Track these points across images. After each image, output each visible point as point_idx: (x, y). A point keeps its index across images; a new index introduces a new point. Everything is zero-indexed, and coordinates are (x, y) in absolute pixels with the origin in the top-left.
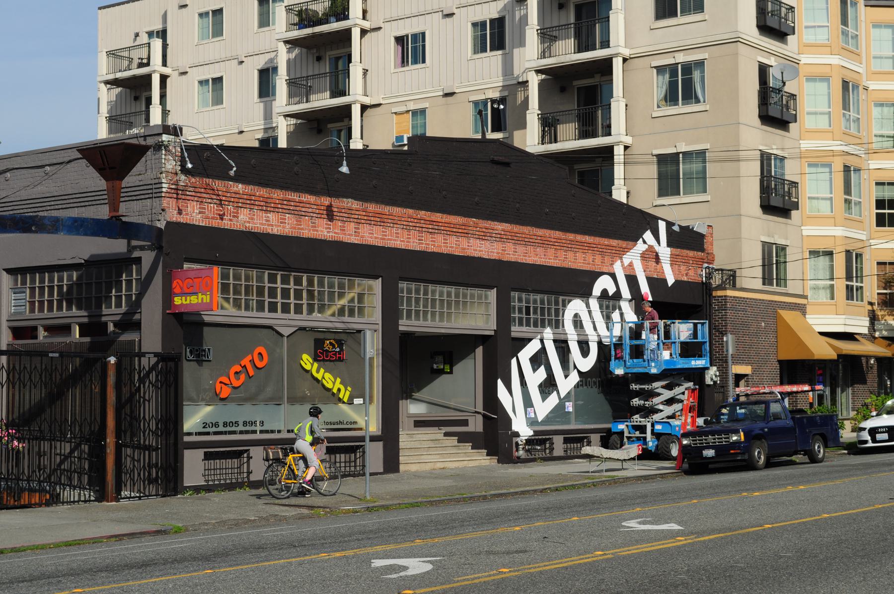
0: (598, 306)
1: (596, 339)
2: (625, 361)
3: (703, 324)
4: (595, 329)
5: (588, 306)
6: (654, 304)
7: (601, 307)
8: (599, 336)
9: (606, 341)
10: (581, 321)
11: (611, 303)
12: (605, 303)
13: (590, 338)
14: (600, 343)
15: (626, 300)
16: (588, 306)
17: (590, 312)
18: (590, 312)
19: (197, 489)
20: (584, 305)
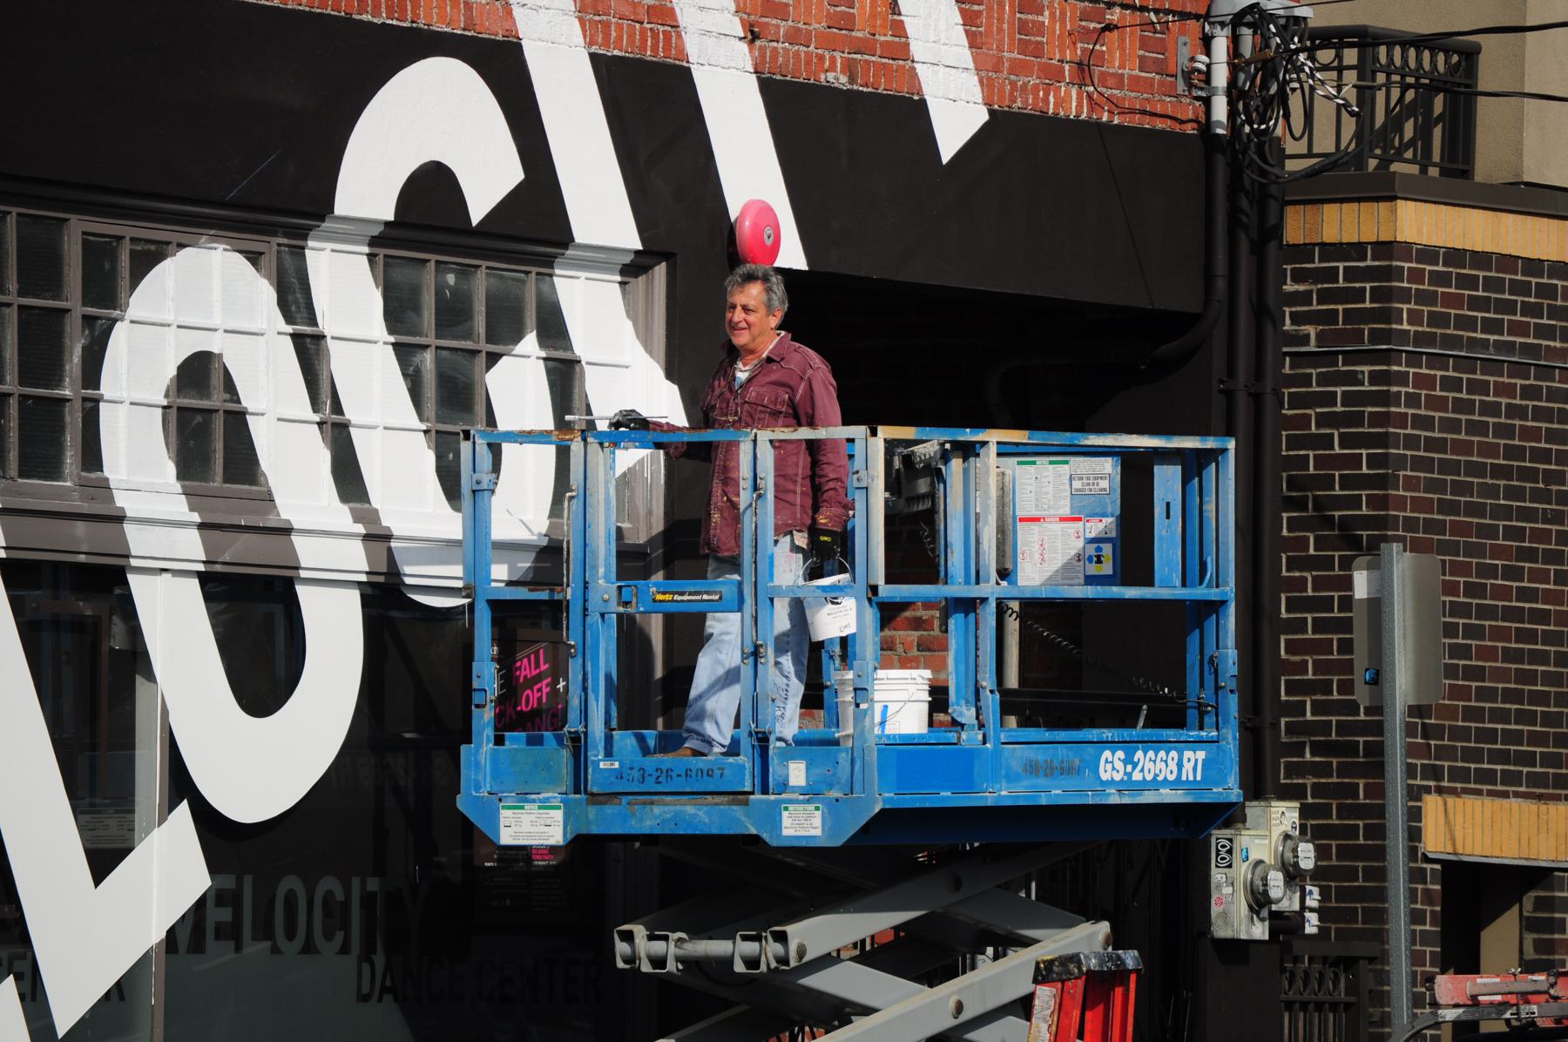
1: (355, 559)
2: (578, 745)
5: (294, 298)
7: (398, 312)
8: (377, 538)
9: (434, 580)
10: (237, 421)
12: (433, 279)
13: (309, 553)
14: (385, 600)
15: (598, 259)
16: (294, 298)
20: (265, 292)
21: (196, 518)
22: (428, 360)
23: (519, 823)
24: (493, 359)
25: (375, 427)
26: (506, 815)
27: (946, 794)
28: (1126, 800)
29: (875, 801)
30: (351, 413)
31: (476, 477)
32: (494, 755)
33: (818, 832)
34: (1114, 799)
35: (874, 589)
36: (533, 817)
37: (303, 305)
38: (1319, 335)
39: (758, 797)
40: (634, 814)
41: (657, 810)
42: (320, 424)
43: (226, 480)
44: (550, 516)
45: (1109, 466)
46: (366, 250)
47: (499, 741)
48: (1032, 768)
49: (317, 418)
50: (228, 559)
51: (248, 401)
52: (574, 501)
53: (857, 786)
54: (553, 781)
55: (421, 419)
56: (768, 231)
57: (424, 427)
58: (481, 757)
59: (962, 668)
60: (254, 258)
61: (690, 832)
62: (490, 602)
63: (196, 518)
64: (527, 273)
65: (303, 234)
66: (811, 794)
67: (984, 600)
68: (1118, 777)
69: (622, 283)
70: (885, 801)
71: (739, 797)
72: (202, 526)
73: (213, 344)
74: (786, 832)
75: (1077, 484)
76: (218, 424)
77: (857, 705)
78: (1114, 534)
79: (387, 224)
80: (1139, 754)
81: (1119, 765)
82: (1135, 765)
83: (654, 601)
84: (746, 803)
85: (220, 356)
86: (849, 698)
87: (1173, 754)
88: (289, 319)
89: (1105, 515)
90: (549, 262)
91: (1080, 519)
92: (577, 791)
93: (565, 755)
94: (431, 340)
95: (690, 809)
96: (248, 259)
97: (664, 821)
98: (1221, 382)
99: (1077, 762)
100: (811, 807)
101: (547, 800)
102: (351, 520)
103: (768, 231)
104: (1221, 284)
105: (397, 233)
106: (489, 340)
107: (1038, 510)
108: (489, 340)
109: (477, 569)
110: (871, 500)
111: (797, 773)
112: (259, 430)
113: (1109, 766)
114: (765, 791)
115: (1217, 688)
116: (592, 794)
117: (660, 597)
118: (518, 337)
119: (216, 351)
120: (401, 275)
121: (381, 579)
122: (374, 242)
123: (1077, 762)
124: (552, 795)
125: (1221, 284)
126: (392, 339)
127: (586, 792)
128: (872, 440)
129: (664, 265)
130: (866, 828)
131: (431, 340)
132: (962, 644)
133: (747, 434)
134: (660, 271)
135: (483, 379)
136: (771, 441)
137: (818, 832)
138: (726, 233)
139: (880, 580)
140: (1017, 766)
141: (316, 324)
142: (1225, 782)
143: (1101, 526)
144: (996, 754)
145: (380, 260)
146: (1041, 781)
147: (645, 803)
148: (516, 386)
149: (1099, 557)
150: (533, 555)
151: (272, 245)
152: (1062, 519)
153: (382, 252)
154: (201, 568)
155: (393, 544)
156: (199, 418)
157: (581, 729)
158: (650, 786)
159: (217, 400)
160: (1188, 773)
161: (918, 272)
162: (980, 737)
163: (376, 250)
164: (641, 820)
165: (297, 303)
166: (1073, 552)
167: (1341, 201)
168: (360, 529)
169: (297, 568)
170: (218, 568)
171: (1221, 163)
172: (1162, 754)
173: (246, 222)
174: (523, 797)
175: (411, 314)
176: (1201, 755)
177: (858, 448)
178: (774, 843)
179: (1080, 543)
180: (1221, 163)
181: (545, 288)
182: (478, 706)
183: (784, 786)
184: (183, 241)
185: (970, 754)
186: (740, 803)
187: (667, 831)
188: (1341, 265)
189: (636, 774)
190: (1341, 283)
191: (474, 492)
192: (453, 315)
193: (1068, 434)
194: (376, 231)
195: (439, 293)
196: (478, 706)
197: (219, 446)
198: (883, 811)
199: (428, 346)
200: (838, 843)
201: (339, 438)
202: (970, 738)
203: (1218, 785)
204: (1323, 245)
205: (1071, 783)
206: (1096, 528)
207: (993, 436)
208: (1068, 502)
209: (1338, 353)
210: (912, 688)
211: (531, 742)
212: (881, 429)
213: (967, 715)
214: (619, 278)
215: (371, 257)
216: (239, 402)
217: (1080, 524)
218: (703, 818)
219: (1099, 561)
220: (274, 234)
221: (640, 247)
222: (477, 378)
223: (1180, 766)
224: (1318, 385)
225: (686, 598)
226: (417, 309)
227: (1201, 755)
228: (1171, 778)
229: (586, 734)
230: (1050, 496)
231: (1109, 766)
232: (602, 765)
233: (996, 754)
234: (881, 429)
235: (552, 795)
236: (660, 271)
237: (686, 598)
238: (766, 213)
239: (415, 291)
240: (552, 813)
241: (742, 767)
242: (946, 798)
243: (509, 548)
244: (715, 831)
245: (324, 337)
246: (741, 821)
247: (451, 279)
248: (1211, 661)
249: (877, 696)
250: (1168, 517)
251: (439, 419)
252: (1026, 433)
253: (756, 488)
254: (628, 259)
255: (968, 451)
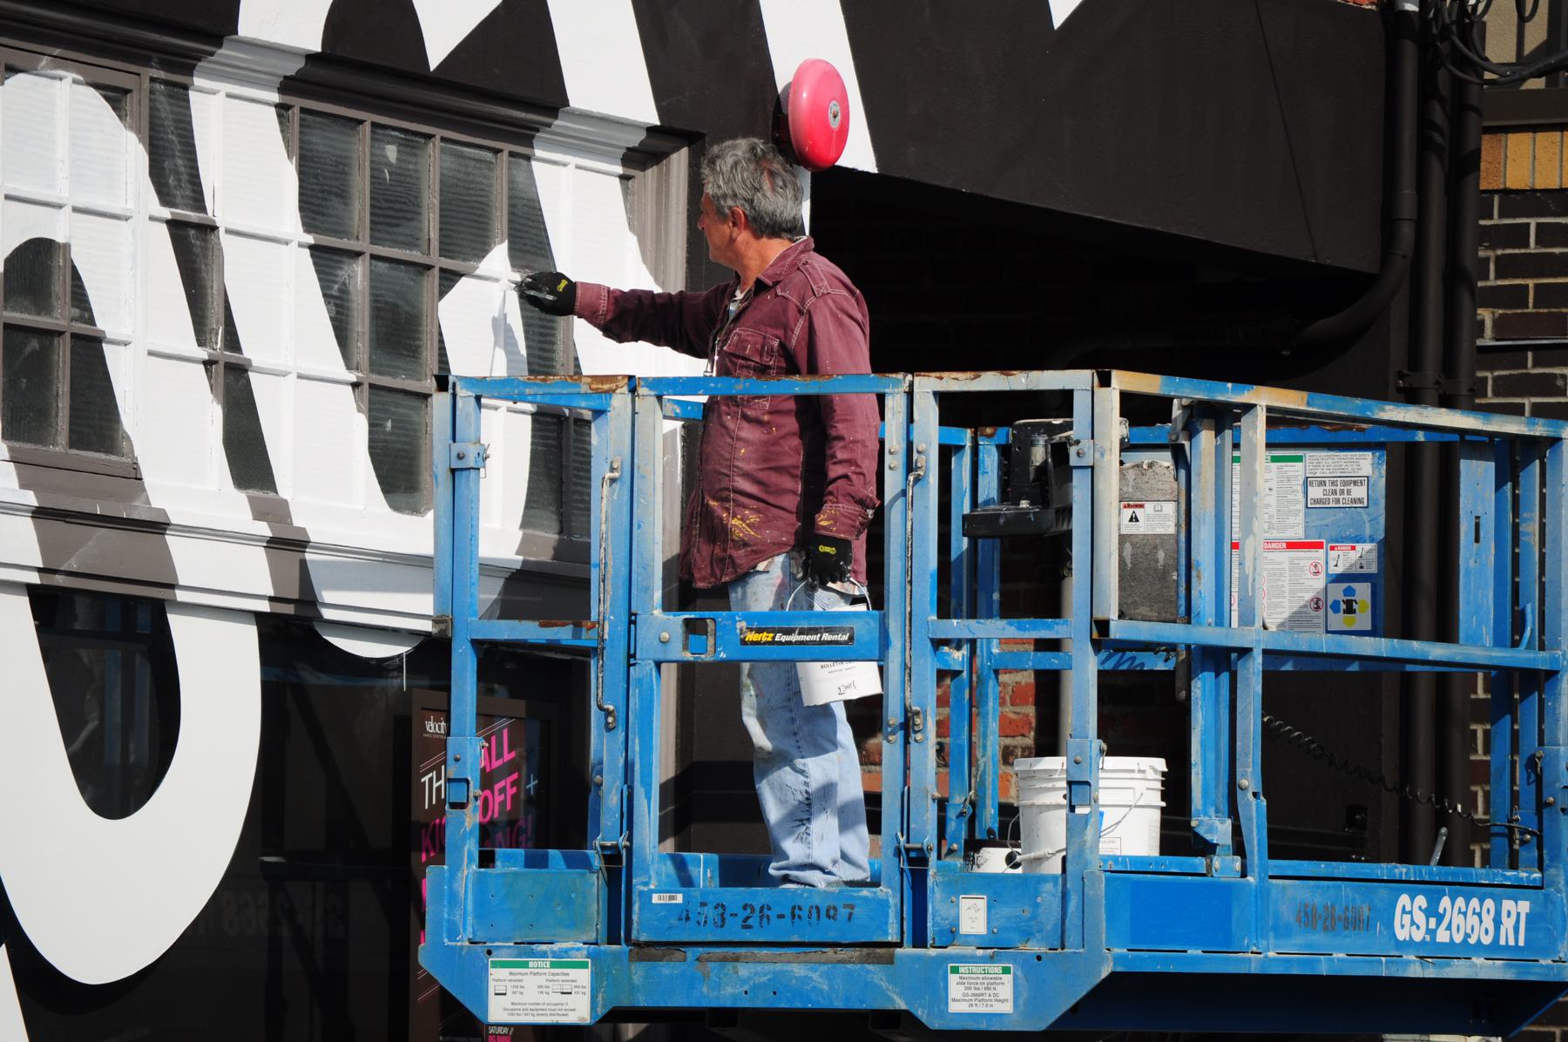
0: (286, 178)
1: (253, 577)
2: (618, 866)
3: (1514, 457)
4: (248, 457)
5: (173, 165)
6: (850, 215)
7: (318, 201)
8: (287, 545)
9: (375, 615)
10: (90, 348)
11: (435, 163)
12: (369, 151)
13: (193, 564)
14: (292, 639)
15: (594, 135)
16: (173, 165)
17: (194, 245)
18: (194, 245)
19: (80, 634)
20: (132, 153)
21: (30, 499)
22: (358, 275)
23: (518, 989)
24: (449, 279)
25: (284, 374)
26: (498, 977)
27: (1195, 952)
28: (1430, 973)
29: (1102, 961)
30: (251, 350)
31: (456, 448)
32: (480, 883)
33: (1007, 1008)
34: (1415, 970)
35: (1103, 626)
36: (541, 980)
37: (185, 177)
38: (1499, 324)
39: (907, 950)
40: (706, 976)
41: (744, 970)
42: (208, 364)
43: (75, 442)
44: (523, 526)
45: (1366, 464)
46: (275, 97)
47: (486, 859)
48: (1309, 917)
49: (203, 354)
50: (74, 567)
51: (106, 321)
52: (616, 486)
53: (1072, 937)
54: (574, 924)
55: (349, 367)
56: (834, 107)
57: (352, 377)
58: (456, 888)
59: (1211, 757)
60: (115, 97)
61: (798, 1005)
62: (476, 644)
63: (30, 499)
64: (497, 151)
65: (185, 64)
66: (995, 947)
67: (1245, 652)
68: (1418, 936)
69: (624, 178)
70: (1117, 959)
71: (877, 950)
72: (39, 513)
73: (57, 228)
74: (954, 1007)
75: (1315, 492)
76: (63, 354)
77: (1072, 808)
78: (1373, 569)
79: (311, 57)
80: (1445, 902)
81: (1420, 918)
82: (1440, 918)
83: (743, 642)
84: (890, 960)
85: (67, 247)
86: (1058, 798)
87: (1489, 903)
88: (165, 198)
89: (1359, 539)
90: (524, 136)
91: (1319, 546)
92: (613, 939)
93: (593, 885)
94: (363, 244)
95: (799, 970)
96: (107, 99)
97: (755, 987)
98: (1401, 376)
99: (1366, 912)
100: (996, 968)
101: (566, 952)
102: (250, 516)
103: (834, 107)
104: (1407, 231)
105: (323, 73)
106: (445, 251)
107: (1271, 528)
108: (445, 251)
109: (449, 595)
110: (1100, 486)
111: (973, 916)
112: (122, 368)
113: (1407, 918)
114: (920, 941)
115: (1541, 805)
116: (638, 945)
117: (752, 637)
118: (482, 251)
119: (60, 239)
120: (326, 141)
121: (289, 609)
122: (288, 86)
123: (1366, 912)
124: (574, 946)
125: (1407, 231)
126: (310, 239)
127: (628, 940)
128: (1101, 392)
129: (684, 151)
130: (1074, 1009)
131: (363, 244)
132: (1211, 721)
133: (897, 383)
134: (679, 161)
135: (435, 310)
136: (935, 394)
137: (1007, 1008)
138: (771, 108)
139: (1113, 615)
140: (1288, 915)
141: (203, 209)
142: (1556, 952)
143: (1353, 556)
144: (1262, 893)
145: (295, 114)
146: (1318, 939)
147: (724, 959)
148: (476, 317)
149: (1349, 604)
150: (500, 583)
151: (143, 79)
152: (1292, 546)
153: (298, 102)
154: (34, 578)
155: (308, 556)
156: (34, 344)
157: (622, 842)
158: (733, 932)
159: (60, 317)
160: (1507, 936)
161: (1016, 188)
162: (1238, 866)
163: (289, 100)
164: (719, 986)
165: (177, 173)
166: (1308, 596)
167: (1535, 129)
168: (264, 529)
169: (172, 586)
170: (60, 580)
171: (1409, 50)
172: (1475, 902)
173: (106, 38)
174: (527, 948)
175: (335, 201)
176: (1524, 907)
177: (1080, 404)
178: (935, 1024)
179: (1319, 583)
180: (1409, 50)
181: (521, 178)
182: (454, 806)
183: (951, 934)
184: (16, 63)
185: (1227, 888)
186: (878, 960)
187: (759, 1004)
188: (1532, 222)
189: (711, 913)
190: (1533, 247)
191: (453, 471)
192: (394, 209)
193: (1358, 402)
194: (293, 67)
195: (376, 178)
196: (454, 806)
197: (63, 387)
198: (1113, 975)
199: (358, 254)
200: (1040, 1025)
201: (234, 384)
202: (1224, 865)
203: (1546, 954)
204: (1506, 192)
205: (1358, 941)
206: (1346, 558)
207: (1264, 398)
208: (1301, 519)
209: (1526, 348)
210: (1140, 786)
211: (530, 863)
212: (1116, 376)
213: (1218, 830)
214: (619, 170)
215: (282, 109)
216: (91, 321)
217: (1321, 552)
218: (818, 983)
219: (1350, 610)
220: (145, 62)
221: (655, 120)
222: (425, 307)
223: (1497, 922)
224: (1496, 394)
225: (794, 638)
226: (343, 195)
227: (1524, 907)
228: (1487, 940)
229: (629, 849)
230: (1273, 510)
231: (1407, 918)
232: (655, 899)
233: (1262, 893)
234: (1116, 376)
235: (574, 946)
236: (679, 161)
237: (794, 638)
238: (831, 75)
239: (341, 168)
240: (574, 973)
241: (884, 904)
242: (1196, 959)
243: (488, 569)
244: (838, 1004)
245: (214, 228)
246: (882, 989)
247: (391, 152)
248: (1532, 763)
249: (1104, 797)
250: (1477, 540)
251: (375, 367)
252: (1304, 395)
253: (910, 467)
254: (635, 139)
255: (1223, 417)
